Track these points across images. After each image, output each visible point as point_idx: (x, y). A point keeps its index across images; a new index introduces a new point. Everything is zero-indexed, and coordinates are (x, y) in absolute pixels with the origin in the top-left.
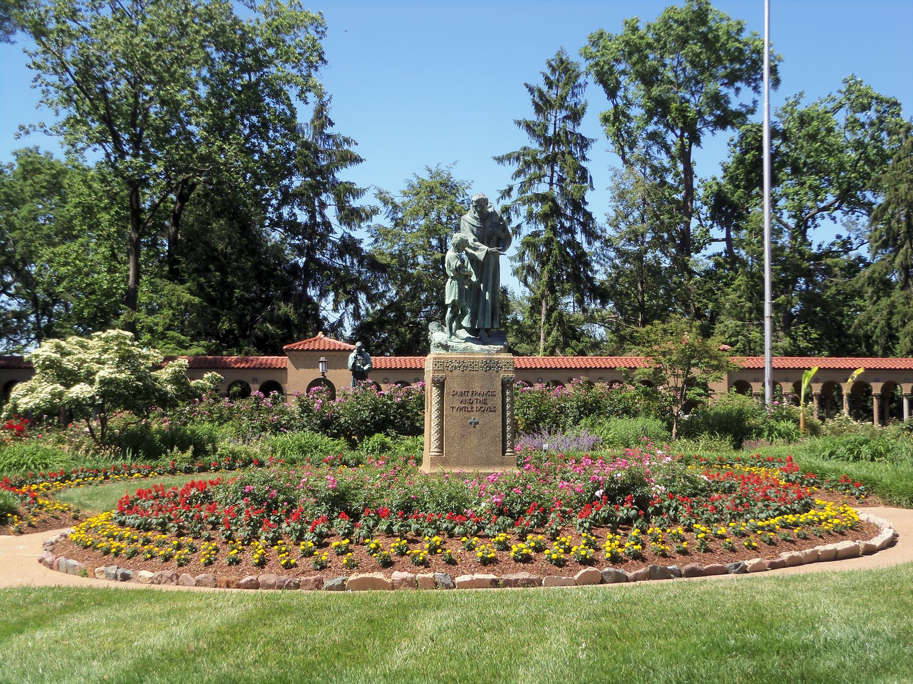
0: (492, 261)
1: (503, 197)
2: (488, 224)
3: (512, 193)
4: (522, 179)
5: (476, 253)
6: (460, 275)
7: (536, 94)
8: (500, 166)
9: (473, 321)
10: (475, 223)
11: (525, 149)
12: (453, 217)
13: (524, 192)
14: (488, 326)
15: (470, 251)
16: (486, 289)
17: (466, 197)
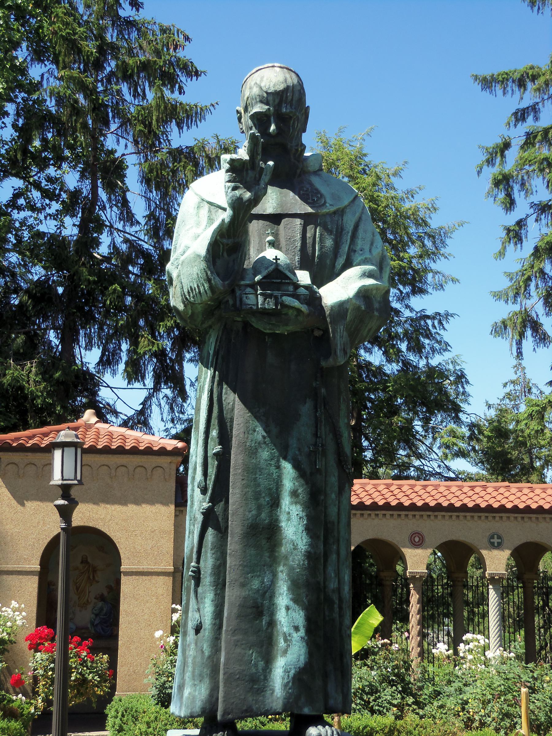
8: (486, 94)
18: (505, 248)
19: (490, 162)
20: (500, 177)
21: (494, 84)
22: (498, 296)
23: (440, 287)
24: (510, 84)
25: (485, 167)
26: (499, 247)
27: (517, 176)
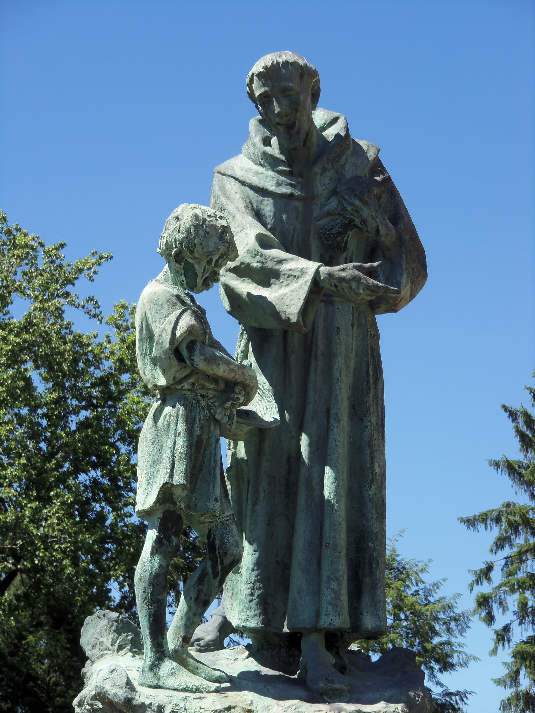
0: (347, 342)
1: (478, 581)
2: (322, 184)
3: (493, 575)
4: (507, 551)
5: (271, 294)
6: (198, 378)
7: (521, 420)
8: (471, 532)
9: (272, 592)
10: (268, 179)
11: (508, 505)
12: (402, 616)
13: (511, 574)
14: (335, 618)
15: (245, 287)
16: (322, 454)
17: (421, 586)
18: (496, 648)
19: (478, 581)
20: (481, 600)
21: (476, 523)
22: (499, 682)
23: (465, 664)
24: (489, 522)
25: (475, 586)
26: (492, 646)
27: (496, 596)
